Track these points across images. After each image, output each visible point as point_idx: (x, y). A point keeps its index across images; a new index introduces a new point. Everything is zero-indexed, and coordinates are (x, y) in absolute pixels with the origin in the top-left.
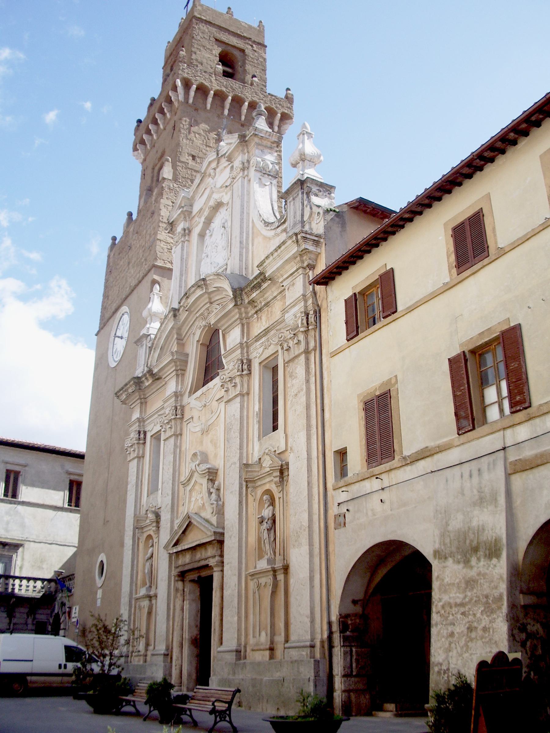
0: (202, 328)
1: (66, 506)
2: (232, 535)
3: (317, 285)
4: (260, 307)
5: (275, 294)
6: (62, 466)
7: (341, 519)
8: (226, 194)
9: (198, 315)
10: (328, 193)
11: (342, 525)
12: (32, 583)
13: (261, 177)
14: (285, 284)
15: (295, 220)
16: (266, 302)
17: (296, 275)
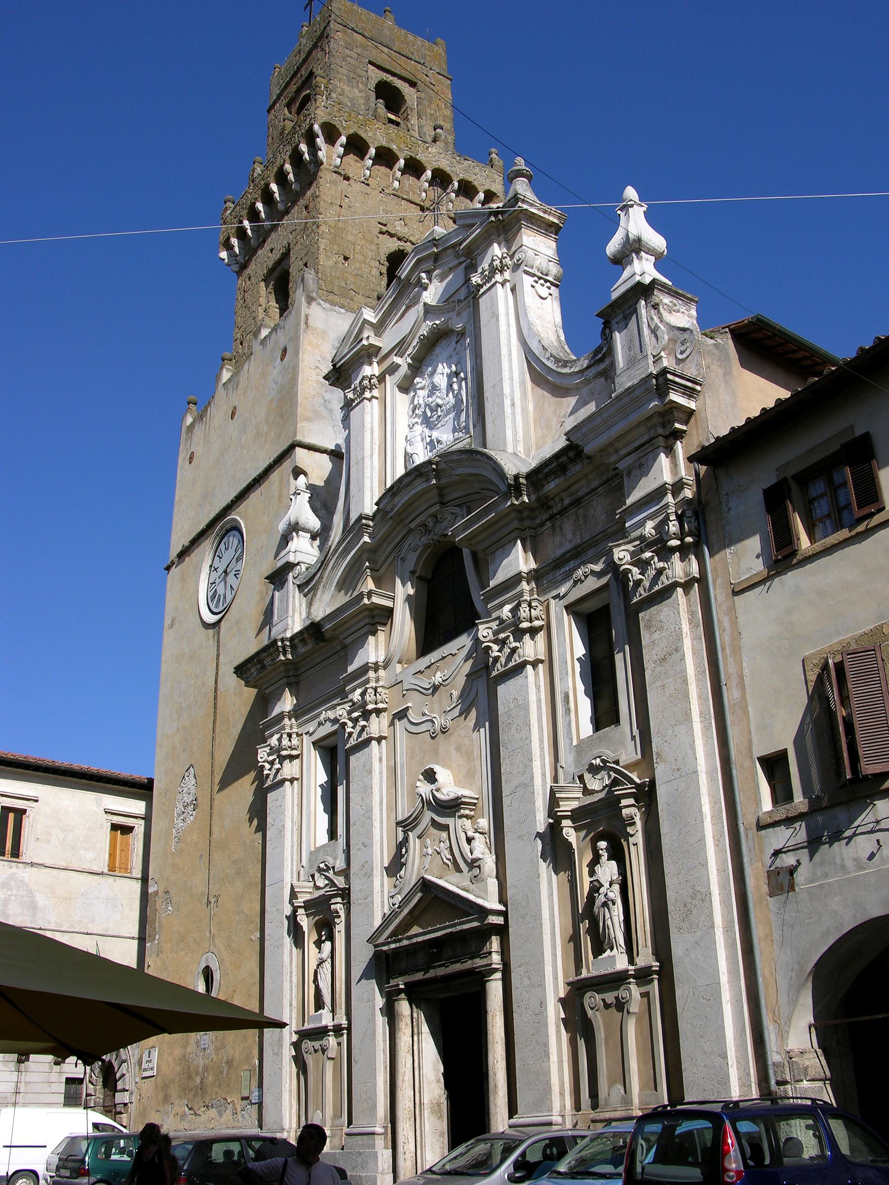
0: (420, 549)
1: (106, 871)
4: (559, 508)
5: (595, 484)
6: (99, 805)
7: (784, 879)
8: (459, 314)
9: (413, 525)
11: (786, 888)
13: (534, 284)
14: (622, 465)
15: (632, 353)
16: (574, 497)
17: (647, 448)
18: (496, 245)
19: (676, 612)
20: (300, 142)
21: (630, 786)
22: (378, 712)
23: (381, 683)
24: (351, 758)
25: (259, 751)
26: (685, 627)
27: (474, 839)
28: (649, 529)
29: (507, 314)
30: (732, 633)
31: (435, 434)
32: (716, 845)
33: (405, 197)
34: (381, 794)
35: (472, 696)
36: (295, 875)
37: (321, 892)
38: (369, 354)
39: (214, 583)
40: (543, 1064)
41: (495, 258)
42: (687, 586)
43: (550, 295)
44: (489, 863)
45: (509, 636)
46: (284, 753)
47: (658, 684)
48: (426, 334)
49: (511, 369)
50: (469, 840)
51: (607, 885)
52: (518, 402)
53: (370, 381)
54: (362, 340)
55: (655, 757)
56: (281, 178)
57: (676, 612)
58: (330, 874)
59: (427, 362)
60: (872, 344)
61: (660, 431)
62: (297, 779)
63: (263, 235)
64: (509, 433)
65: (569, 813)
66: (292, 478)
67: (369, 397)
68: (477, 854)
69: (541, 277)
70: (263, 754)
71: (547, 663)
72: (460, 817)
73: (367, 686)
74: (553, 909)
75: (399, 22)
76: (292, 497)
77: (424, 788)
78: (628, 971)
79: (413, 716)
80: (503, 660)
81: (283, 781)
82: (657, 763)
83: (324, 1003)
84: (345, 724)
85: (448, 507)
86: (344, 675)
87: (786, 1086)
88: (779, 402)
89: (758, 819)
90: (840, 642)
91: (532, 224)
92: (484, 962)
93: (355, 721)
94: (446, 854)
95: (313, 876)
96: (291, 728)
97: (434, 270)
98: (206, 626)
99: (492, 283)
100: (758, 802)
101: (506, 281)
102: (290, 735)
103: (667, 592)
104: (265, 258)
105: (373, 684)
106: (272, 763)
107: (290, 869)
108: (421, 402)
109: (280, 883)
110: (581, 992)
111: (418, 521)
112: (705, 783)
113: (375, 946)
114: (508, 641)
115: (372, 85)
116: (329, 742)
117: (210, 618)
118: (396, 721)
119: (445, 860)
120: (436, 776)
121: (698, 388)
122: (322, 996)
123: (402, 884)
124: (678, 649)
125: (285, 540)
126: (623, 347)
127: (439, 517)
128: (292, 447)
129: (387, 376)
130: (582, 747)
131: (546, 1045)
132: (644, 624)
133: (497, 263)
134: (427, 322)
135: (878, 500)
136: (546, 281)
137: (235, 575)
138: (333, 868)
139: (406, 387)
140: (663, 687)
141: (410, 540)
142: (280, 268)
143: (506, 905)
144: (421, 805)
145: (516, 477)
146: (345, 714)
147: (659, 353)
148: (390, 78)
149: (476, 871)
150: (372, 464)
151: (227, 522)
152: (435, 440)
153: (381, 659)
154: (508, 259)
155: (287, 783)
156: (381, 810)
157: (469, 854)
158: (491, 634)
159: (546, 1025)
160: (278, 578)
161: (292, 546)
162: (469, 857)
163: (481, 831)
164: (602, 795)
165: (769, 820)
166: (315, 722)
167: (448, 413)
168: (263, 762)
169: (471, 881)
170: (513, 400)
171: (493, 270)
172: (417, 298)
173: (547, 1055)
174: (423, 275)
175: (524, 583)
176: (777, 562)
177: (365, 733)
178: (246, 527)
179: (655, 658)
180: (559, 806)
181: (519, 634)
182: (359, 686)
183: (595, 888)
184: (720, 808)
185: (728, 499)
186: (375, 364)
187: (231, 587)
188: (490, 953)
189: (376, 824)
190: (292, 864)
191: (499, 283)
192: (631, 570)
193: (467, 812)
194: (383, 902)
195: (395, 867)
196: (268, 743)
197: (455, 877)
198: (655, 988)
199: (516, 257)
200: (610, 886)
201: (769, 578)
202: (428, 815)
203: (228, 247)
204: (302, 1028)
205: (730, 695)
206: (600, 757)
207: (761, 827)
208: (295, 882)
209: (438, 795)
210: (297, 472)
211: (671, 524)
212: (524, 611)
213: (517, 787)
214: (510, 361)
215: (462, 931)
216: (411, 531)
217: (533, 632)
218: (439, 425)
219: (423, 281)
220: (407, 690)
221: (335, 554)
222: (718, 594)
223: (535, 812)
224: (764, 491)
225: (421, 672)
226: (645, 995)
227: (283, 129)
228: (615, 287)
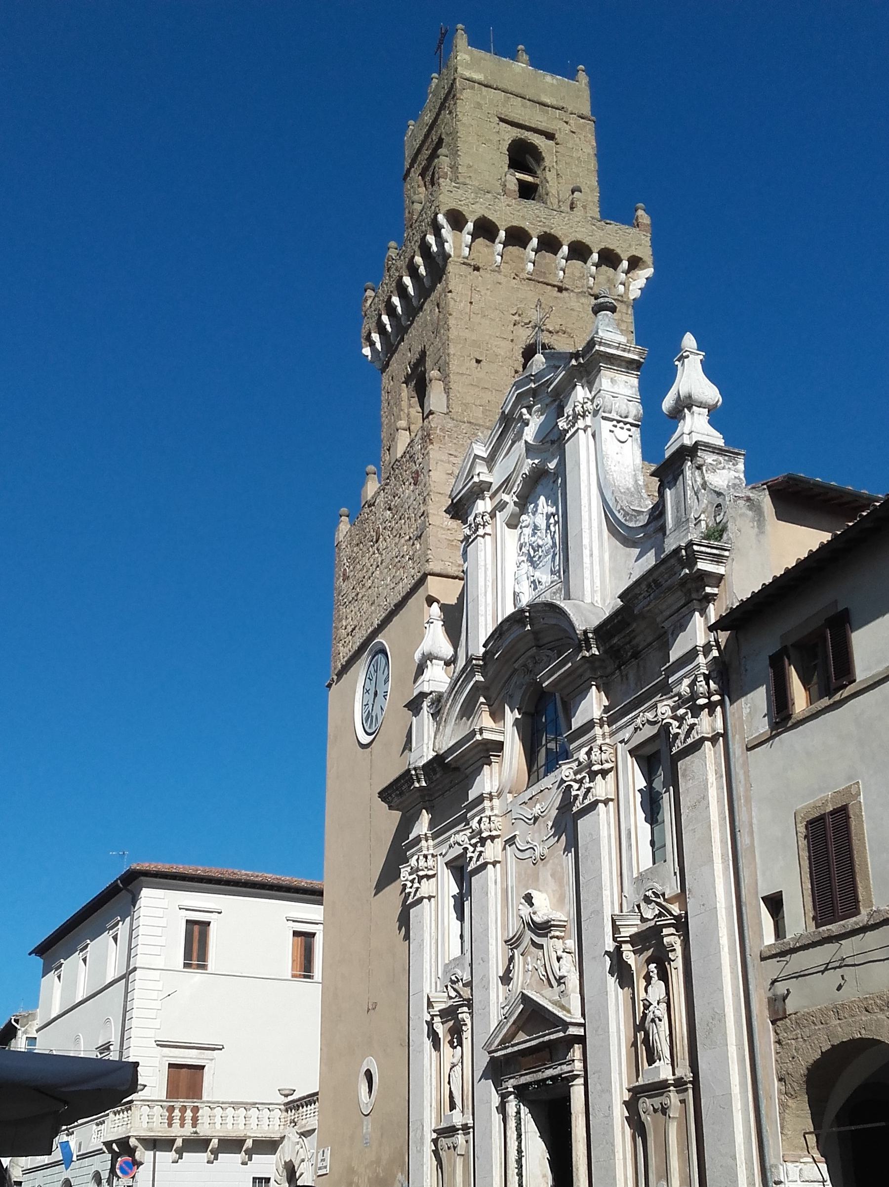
2: (598, 1027)
3: (722, 631)
5: (649, 639)
9: (516, 666)
10: (733, 465)
12: (254, 1112)
13: (613, 429)
14: (666, 625)
18: (579, 388)
21: (669, 917)
23: (496, 812)
24: (473, 878)
25: (402, 870)
26: (712, 778)
27: (561, 958)
28: (684, 688)
30: (746, 784)
31: (538, 574)
35: (563, 826)
38: (479, 490)
41: (576, 404)
42: (714, 740)
43: (630, 436)
45: (585, 776)
46: (421, 873)
47: (690, 828)
48: (528, 473)
51: (655, 1004)
52: (596, 552)
53: (482, 518)
54: (473, 477)
55: (687, 893)
59: (530, 499)
60: (818, 547)
62: (434, 897)
63: (401, 330)
64: (587, 583)
65: (438, 1013)
66: (426, 605)
67: (482, 534)
68: (563, 972)
70: (405, 872)
71: (616, 801)
72: (551, 938)
73: (482, 815)
77: (525, 910)
80: (682, 737)
81: (422, 899)
85: (543, 649)
86: (466, 803)
88: (823, 547)
90: (821, 799)
91: (612, 364)
92: (566, 1068)
93: (475, 846)
97: (533, 406)
98: (364, 746)
99: (575, 429)
102: (426, 857)
103: (697, 745)
105: (488, 813)
106: (412, 881)
111: (520, 661)
112: (724, 917)
113: (489, 1053)
114: (686, 717)
117: (365, 739)
118: (507, 846)
121: (726, 553)
124: (705, 797)
125: (421, 670)
126: (672, 507)
128: (425, 576)
129: (497, 512)
130: (641, 878)
133: (579, 409)
135: (849, 673)
136: (626, 423)
137: (384, 696)
138: (462, 980)
139: (513, 523)
141: (515, 679)
144: (522, 926)
145: (585, 632)
146: (467, 840)
147: (700, 516)
149: (563, 987)
150: (486, 601)
153: (495, 790)
154: (590, 403)
157: (558, 971)
160: (414, 706)
161: (428, 674)
162: (559, 974)
163: (568, 951)
166: (447, 845)
167: (548, 553)
168: (406, 880)
170: (591, 550)
174: (524, 411)
175: (597, 728)
176: (777, 723)
177: (482, 857)
182: (685, 676)
186: (488, 499)
188: (573, 1061)
190: (431, 975)
191: (581, 429)
192: (671, 724)
193: (557, 934)
195: (506, 979)
196: (575, 758)
197: (547, 991)
199: (596, 402)
200: (658, 1004)
201: (772, 738)
202: (529, 935)
205: (743, 840)
209: (535, 918)
210: (430, 601)
212: (596, 755)
214: (590, 510)
215: (550, 1040)
216: (516, 670)
218: (540, 565)
219: (524, 417)
220: (515, 819)
221: (450, 696)
222: (737, 749)
224: (770, 657)
228: (668, 445)
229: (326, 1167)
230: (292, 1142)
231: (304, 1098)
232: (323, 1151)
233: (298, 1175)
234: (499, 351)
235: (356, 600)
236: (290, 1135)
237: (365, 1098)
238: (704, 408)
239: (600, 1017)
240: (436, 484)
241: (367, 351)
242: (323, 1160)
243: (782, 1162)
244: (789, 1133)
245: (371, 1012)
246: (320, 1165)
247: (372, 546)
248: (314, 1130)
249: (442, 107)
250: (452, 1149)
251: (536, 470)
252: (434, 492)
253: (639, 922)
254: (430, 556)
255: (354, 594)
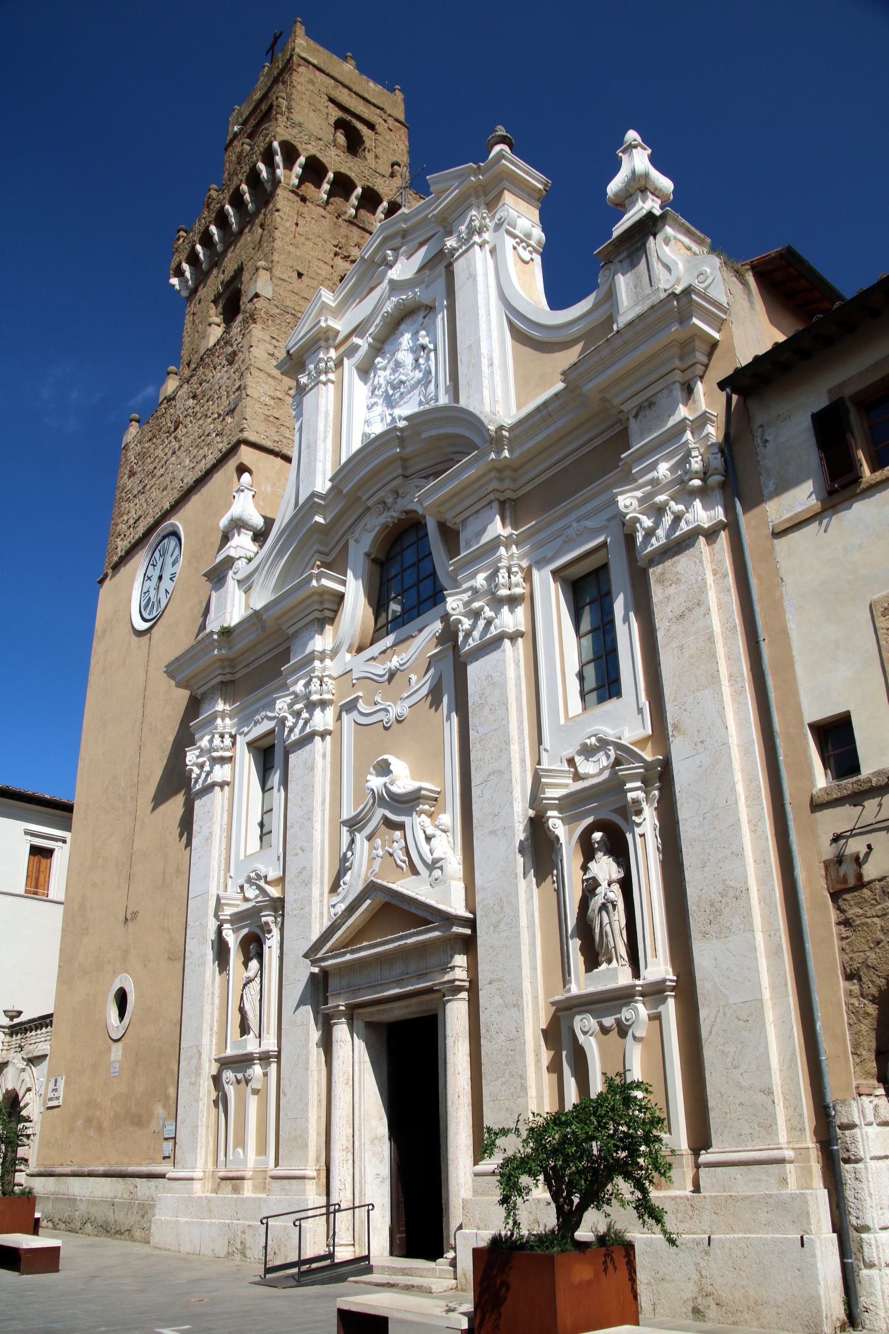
2: (500, 922)
13: (516, 245)
19: (697, 561)
20: (258, 161)
22: (323, 704)
23: (327, 673)
25: (188, 754)
27: (434, 836)
29: (486, 275)
32: (753, 831)
33: (361, 225)
34: (324, 793)
36: (222, 887)
37: (249, 905)
39: (148, 591)
40: (519, 1100)
41: (473, 218)
44: (454, 864)
46: (215, 754)
47: (674, 644)
48: (390, 311)
49: (489, 329)
50: (428, 839)
51: (604, 884)
56: (237, 200)
57: (697, 561)
58: (262, 883)
61: (677, 363)
63: (216, 260)
65: (229, 918)
69: (524, 240)
74: (533, 916)
75: (358, 67)
76: (235, 494)
77: (376, 782)
78: (635, 986)
79: (362, 706)
81: (213, 785)
82: (673, 736)
83: (249, 1028)
84: (285, 718)
87: (853, 1131)
89: (812, 797)
94: (400, 855)
95: (242, 887)
96: (224, 728)
97: (401, 247)
98: (139, 634)
100: (810, 776)
101: (485, 242)
104: (215, 283)
107: (216, 880)
108: (382, 381)
109: (204, 895)
110: (570, 1012)
115: (332, 120)
116: (266, 743)
117: (141, 626)
118: (344, 714)
119: (399, 862)
120: (391, 768)
122: (247, 1019)
123: (346, 891)
125: (226, 538)
127: (400, 492)
129: (345, 359)
131: (523, 1077)
132: (655, 578)
134: (392, 298)
137: (171, 579)
138: (266, 877)
140: (681, 647)
141: (366, 519)
142: (232, 287)
143: (474, 914)
144: (372, 801)
146: (286, 707)
148: (349, 118)
149: (437, 873)
151: (165, 528)
152: (397, 417)
153: (329, 647)
155: (217, 789)
156: (323, 811)
158: (461, 606)
159: (523, 1054)
162: (429, 858)
163: (443, 827)
164: (606, 775)
165: (827, 798)
168: (191, 765)
169: (431, 885)
171: (471, 231)
172: (384, 274)
173: (524, 1088)
178: (185, 530)
179: (670, 615)
180: (544, 793)
181: (311, 706)
183: (590, 887)
184: (758, 786)
185: (763, 431)
187: (166, 591)
189: (318, 826)
190: (219, 874)
193: (426, 807)
194: (322, 913)
198: (670, 1008)
203: (179, 273)
204: (223, 1055)
206: (595, 735)
207: (816, 806)
208: (222, 894)
211: (693, 461)
213: (490, 774)
214: (489, 321)
216: (368, 509)
217: (513, 601)
218: (402, 402)
220: (357, 679)
223: (512, 802)
225: (373, 659)
226: (656, 1018)
227: (242, 151)
229: (58, 1098)
230: (17, 1069)
231: (34, 1020)
232: (56, 1081)
233: (22, 1104)
234: (320, 271)
235: (143, 493)
236: (15, 1061)
237: (115, 1020)
238: (658, 197)
239: (502, 907)
240: (256, 360)
241: (174, 281)
242: (55, 1090)
243: (855, 1095)
244: (864, 1053)
245: (130, 923)
246: (50, 1095)
247: (167, 438)
248: (45, 1056)
249: (276, 81)
250: (243, 1083)
251: (402, 307)
252: (254, 367)
253: (571, 781)
254: (245, 426)
255: (140, 488)
